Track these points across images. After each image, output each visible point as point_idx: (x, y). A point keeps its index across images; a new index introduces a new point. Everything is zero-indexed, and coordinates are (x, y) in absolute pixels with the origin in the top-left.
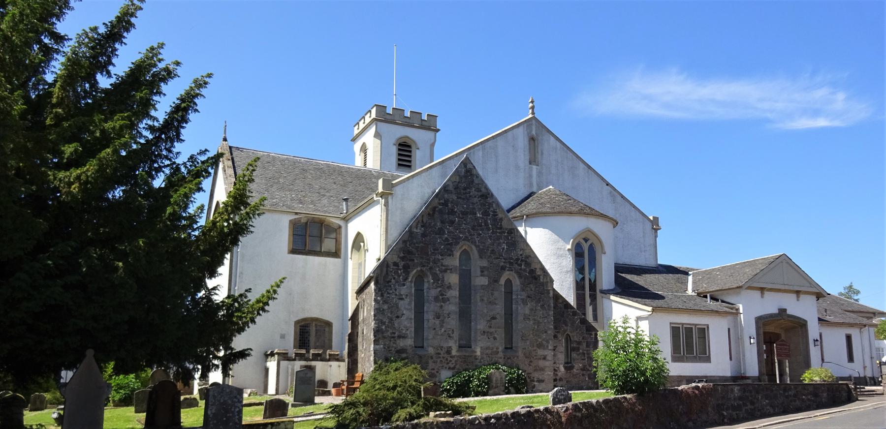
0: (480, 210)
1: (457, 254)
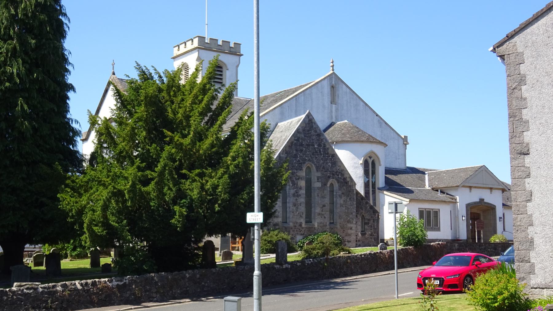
0: (316, 143)
1: (304, 169)
